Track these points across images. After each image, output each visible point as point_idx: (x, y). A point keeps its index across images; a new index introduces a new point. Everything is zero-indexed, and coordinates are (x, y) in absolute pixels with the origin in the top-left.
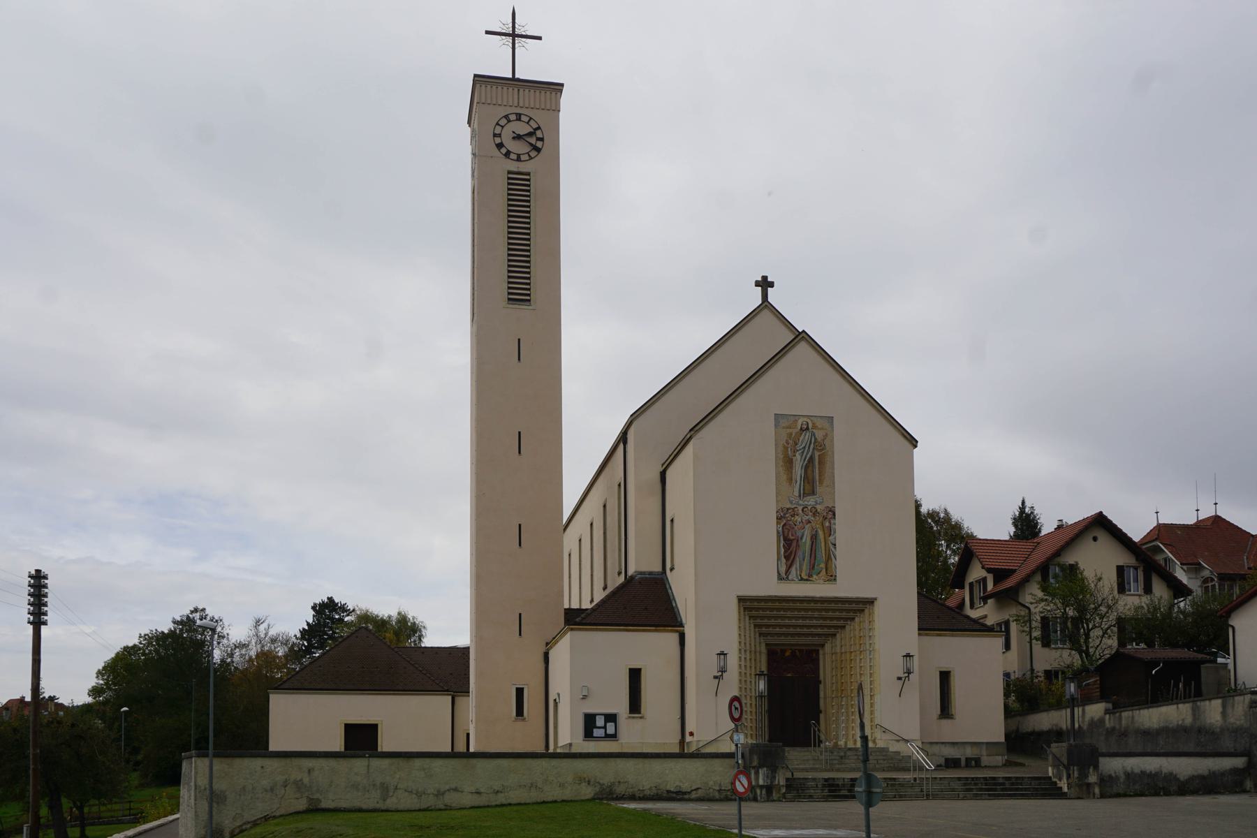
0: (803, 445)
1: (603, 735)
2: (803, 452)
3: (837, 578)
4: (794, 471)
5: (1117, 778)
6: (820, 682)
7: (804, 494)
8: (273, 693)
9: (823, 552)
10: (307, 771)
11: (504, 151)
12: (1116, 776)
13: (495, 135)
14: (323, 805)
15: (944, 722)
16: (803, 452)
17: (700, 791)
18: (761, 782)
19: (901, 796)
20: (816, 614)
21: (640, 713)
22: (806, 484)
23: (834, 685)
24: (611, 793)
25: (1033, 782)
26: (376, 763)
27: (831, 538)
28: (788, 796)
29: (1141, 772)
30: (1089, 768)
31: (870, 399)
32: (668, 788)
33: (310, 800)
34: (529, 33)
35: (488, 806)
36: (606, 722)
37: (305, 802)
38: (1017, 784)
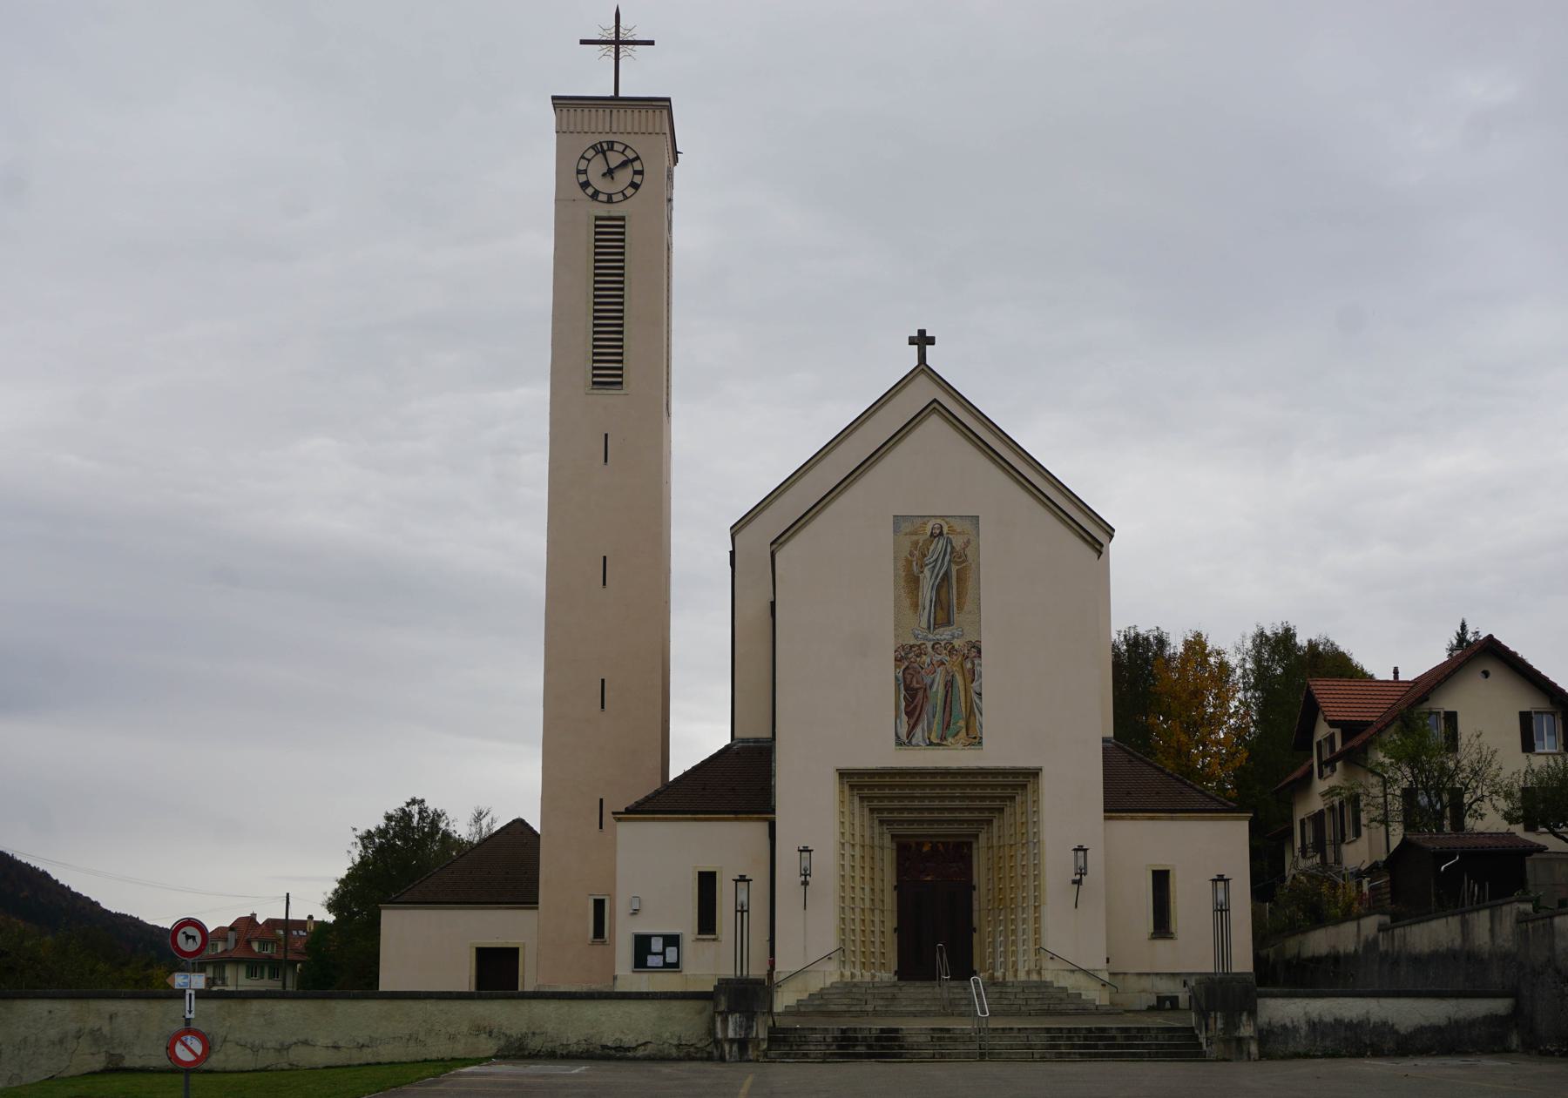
0: (934, 557)
1: (661, 964)
2: (934, 567)
3: (984, 741)
5: (1296, 1029)
6: (974, 888)
7: (935, 624)
8: (386, 908)
9: (963, 705)
10: (107, 1017)
11: (590, 191)
12: (1294, 1027)
13: (579, 172)
14: (127, 1063)
15: (1161, 944)
16: (934, 567)
17: (650, 1046)
18: (731, 1034)
19: (942, 1056)
20: (958, 792)
22: (938, 608)
23: (991, 892)
24: (521, 1048)
25: (1160, 1036)
26: (373, 1007)
27: (974, 684)
28: (772, 1054)
29: (1335, 1020)
30: (1241, 1015)
31: (788, 483)
33: (110, 1056)
34: (637, 38)
35: (349, 1066)
36: (665, 946)
37: (104, 1059)
38: (1136, 1038)
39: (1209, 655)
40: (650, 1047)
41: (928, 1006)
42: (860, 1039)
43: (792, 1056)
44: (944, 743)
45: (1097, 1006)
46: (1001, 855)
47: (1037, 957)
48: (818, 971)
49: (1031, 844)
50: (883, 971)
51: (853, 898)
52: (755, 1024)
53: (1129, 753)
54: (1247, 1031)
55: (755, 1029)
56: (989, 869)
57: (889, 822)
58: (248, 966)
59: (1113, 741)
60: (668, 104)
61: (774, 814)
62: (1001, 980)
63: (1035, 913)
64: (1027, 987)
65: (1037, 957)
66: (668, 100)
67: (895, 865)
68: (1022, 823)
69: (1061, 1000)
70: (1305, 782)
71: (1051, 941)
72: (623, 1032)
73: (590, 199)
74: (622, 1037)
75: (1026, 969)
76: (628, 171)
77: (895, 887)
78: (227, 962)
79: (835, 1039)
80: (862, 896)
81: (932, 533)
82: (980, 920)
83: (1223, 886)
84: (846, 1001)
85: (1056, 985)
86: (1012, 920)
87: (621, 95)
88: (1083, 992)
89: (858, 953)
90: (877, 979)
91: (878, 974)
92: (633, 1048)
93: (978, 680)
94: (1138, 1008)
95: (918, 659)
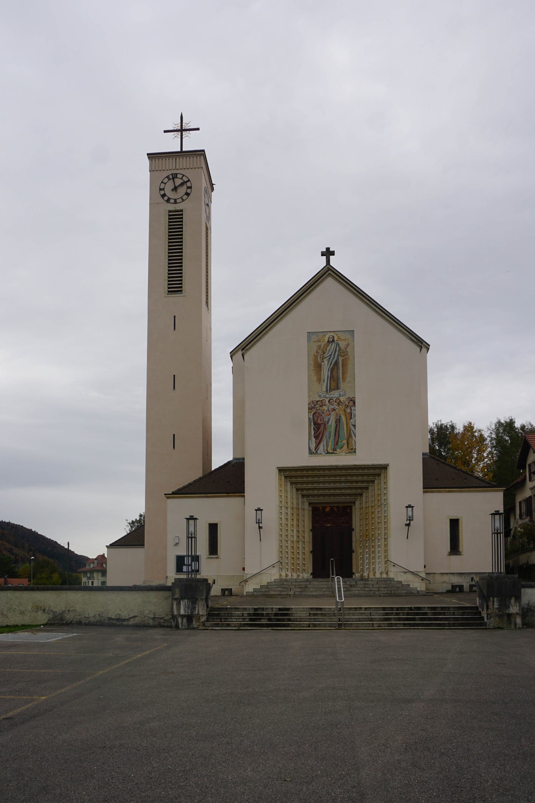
0: (330, 353)
2: (330, 358)
3: (357, 450)
4: (322, 373)
7: (330, 389)
9: (345, 432)
11: (166, 198)
13: (160, 190)
15: (454, 557)
18: (182, 612)
20: (343, 479)
21: (217, 555)
24: (62, 619)
27: (351, 420)
30: (510, 599)
32: (110, 615)
34: (191, 127)
38: (440, 614)
39: (475, 432)
40: (137, 619)
41: (324, 592)
42: (265, 615)
43: (220, 625)
44: (335, 452)
45: (418, 591)
46: (367, 512)
47: (386, 565)
48: (267, 573)
49: (383, 505)
50: (304, 573)
51: (287, 535)
52: (197, 606)
53: (438, 460)
54: (514, 609)
55: (197, 609)
56: (361, 520)
57: (307, 496)
58: (102, 573)
59: (429, 454)
60: (203, 153)
61: (244, 493)
62: (366, 577)
63: (385, 542)
64: (380, 581)
65: (386, 565)
66: (203, 151)
67: (311, 518)
68: (378, 495)
69: (398, 588)
70: (523, 483)
71: (393, 557)
72: (121, 610)
73: (166, 202)
74: (120, 613)
75: (380, 571)
76: (185, 187)
77: (311, 530)
78: (95, 571)
79: (249, 615)
80: (292, 534)
81: (328, 340)
82: (356, 546)
83: (499, 518)
84: (280, 589)
85: (396, 580)
86: (373, 546)
87: (184, 150)
88: (410, 584)
89: (289, 564)
90: (300, 577)
91: (301, 575)
92: (127, 619)
93: (354, 418)
94: (440, 591)
95: (321, 408)
